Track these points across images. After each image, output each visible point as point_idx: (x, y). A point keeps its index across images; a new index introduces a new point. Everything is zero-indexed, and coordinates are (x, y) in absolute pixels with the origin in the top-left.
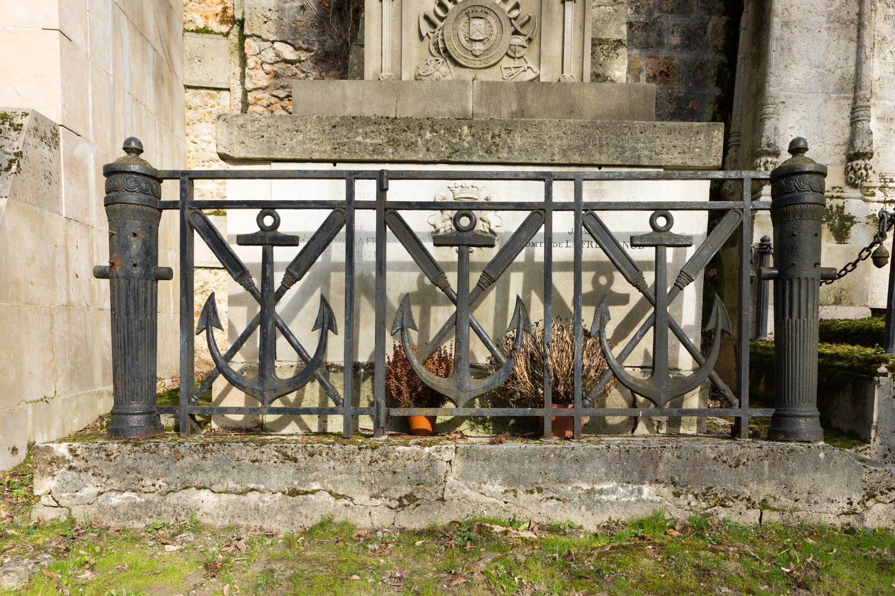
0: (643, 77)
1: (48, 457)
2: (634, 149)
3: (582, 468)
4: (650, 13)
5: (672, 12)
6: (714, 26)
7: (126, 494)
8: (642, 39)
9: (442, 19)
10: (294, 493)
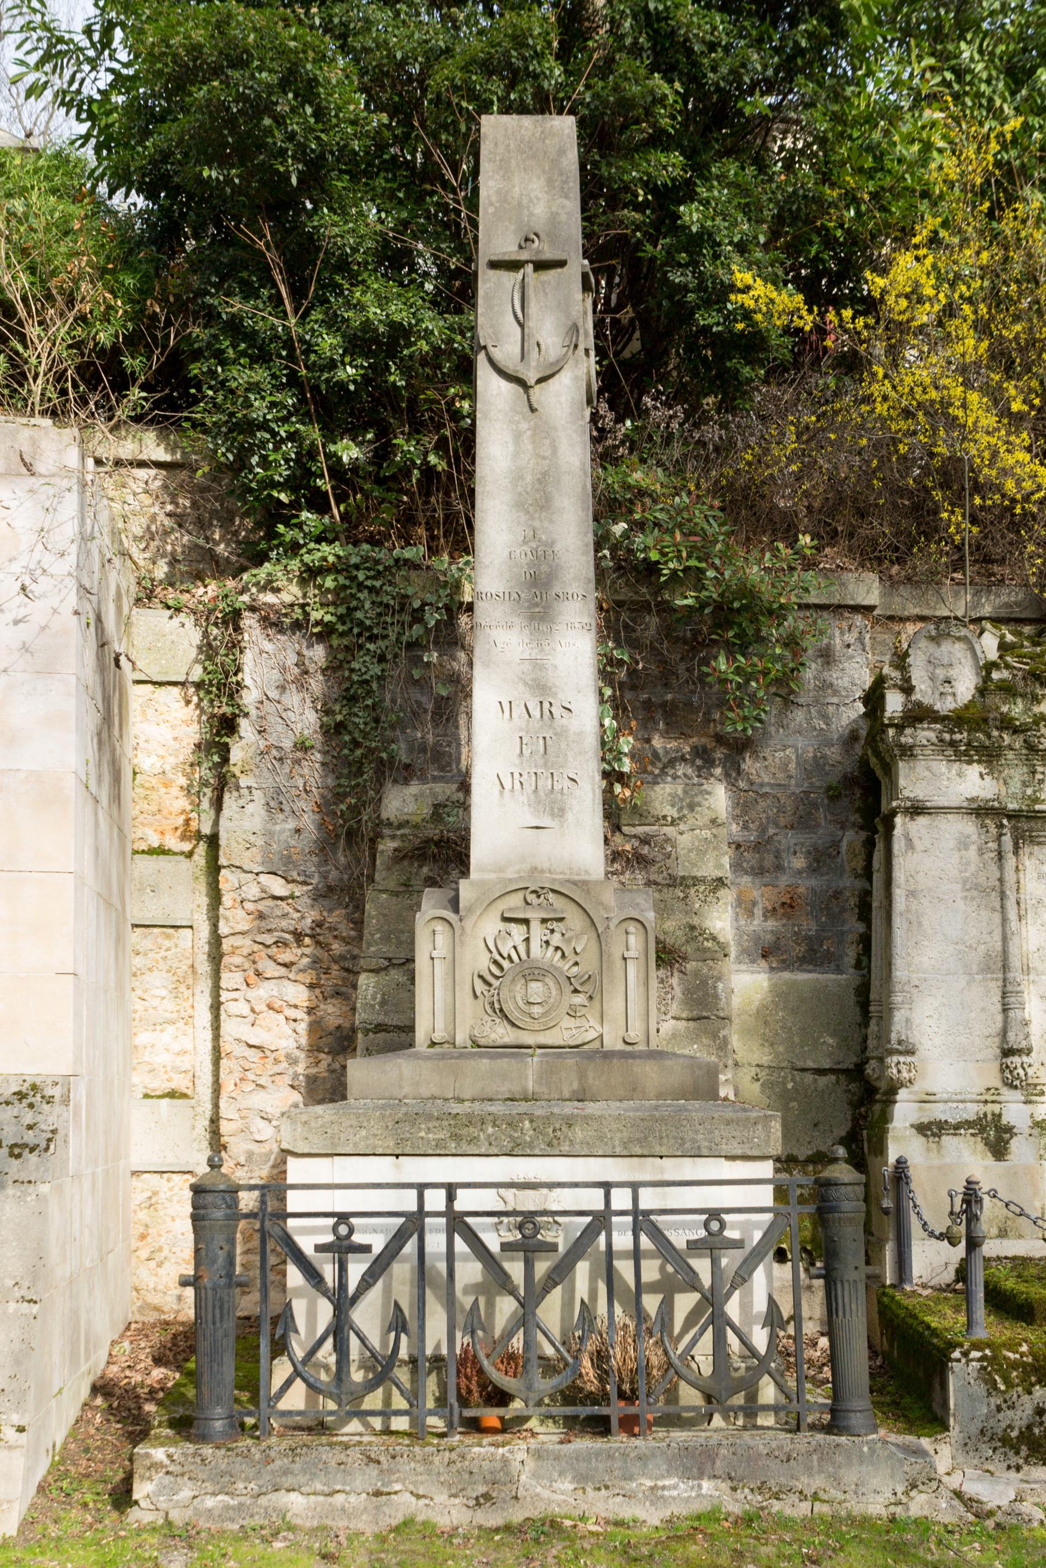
0: (758, 912)
1: (148, 1463)
2: (694, 1141)
3: (645, 1465)
4: (763, 830)
5: (792, 827)
6: (850, 844)
7: (220, 1497)
8: (753, 862)
9: (497, 978)
10: (378, 1494)
